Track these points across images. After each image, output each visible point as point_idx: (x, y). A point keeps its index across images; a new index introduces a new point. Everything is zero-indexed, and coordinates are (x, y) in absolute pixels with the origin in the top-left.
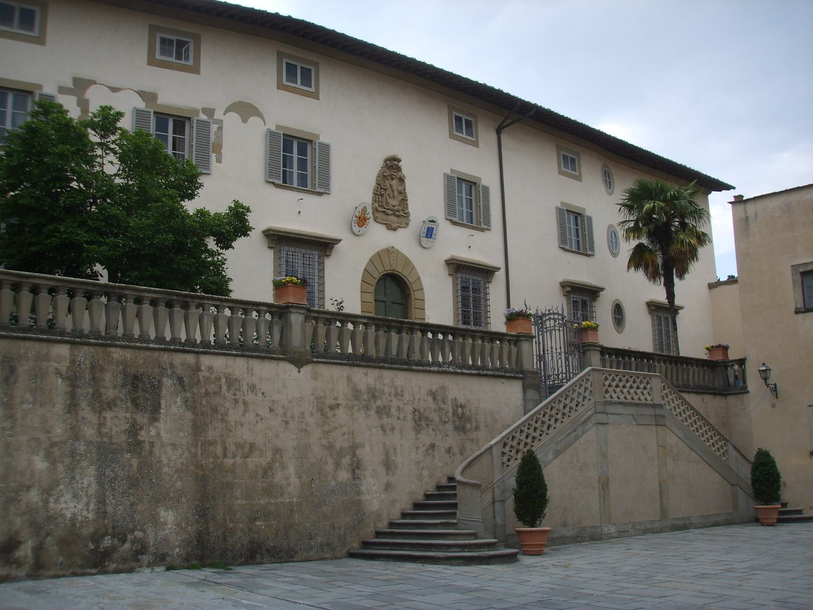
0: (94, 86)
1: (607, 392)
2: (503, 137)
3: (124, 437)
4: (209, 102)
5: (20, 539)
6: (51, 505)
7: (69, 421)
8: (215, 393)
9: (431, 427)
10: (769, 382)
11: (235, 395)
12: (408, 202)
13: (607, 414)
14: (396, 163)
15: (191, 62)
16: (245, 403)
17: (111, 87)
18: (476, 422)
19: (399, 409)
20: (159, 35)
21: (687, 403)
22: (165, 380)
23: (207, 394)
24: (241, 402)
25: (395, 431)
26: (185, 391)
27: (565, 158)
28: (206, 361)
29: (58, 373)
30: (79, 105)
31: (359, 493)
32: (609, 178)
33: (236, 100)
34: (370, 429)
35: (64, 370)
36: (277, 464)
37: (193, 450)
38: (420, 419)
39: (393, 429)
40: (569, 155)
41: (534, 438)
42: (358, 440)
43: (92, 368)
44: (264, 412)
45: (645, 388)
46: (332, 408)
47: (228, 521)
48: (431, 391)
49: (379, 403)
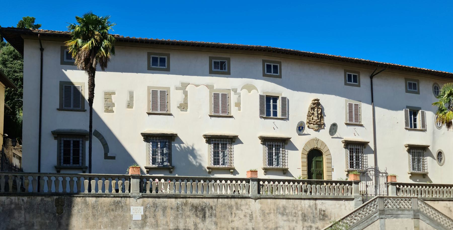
1: (386, 205)
15: (227, 70)
17: (196, 85)
40: (412, 82)
46: (268, 214)
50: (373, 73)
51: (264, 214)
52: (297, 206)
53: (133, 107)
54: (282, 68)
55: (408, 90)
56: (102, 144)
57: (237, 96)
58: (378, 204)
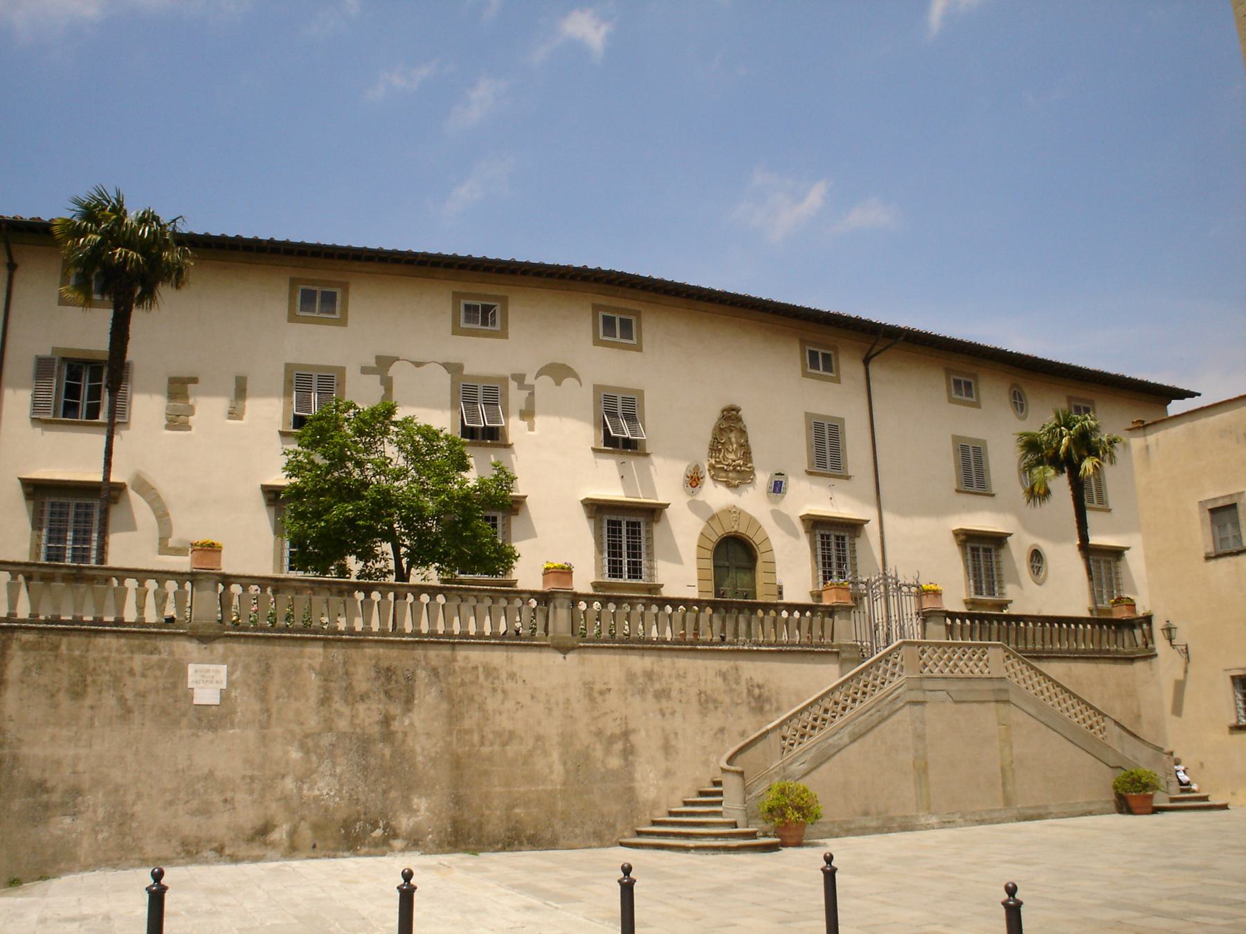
0: (397, 362)
1: (925, 665)
2: (871, 368)
3: (377, 728)
4: (519, 369)
5: (275, 823)
6: (305, 792)
7: (323, 714)
8: (472, 683)
9: (720, 710)
10: (1174, 642)
11: (493, 683)
12: (752, 454)
13: (924, 690)
14: (734, 413)
15: (498, 327)
16: (504, 691)
18: (777, 702)
19: (681, 691)
20: (463, 302)
21: (1041, 673)
22: (418, 671)
23: (463, 684)
24: (499, 691)
25: (677, 714)
26: (440, 681)
27: (957, 383)
28: (461, 654)
29: (311, 667)
30: (382, 383)
31: (632, 779)
32: (1021, 400)
33: (548, 363)
34: (645, 713)
35: (317, 667)
36: (539, 752)
37: (448, 739)
38: (707, 701)
39: (673, 713)
40: (963, 379)
41: (824, 720)
42: (632, 725)
43: (345, 663)
44: (525, 699)
45: (980, 659)
46: (601, 693)
47: (484, 809)
48: (720, 671)
49: (657, 686)
50: (871, 350)
51: (593, 693)
52: (685, 673)
53: (244, 417)
54: (644, 326)
55: (955, 396)
56: (155, 513)
57: (525, 393)
58: (903, 663)
